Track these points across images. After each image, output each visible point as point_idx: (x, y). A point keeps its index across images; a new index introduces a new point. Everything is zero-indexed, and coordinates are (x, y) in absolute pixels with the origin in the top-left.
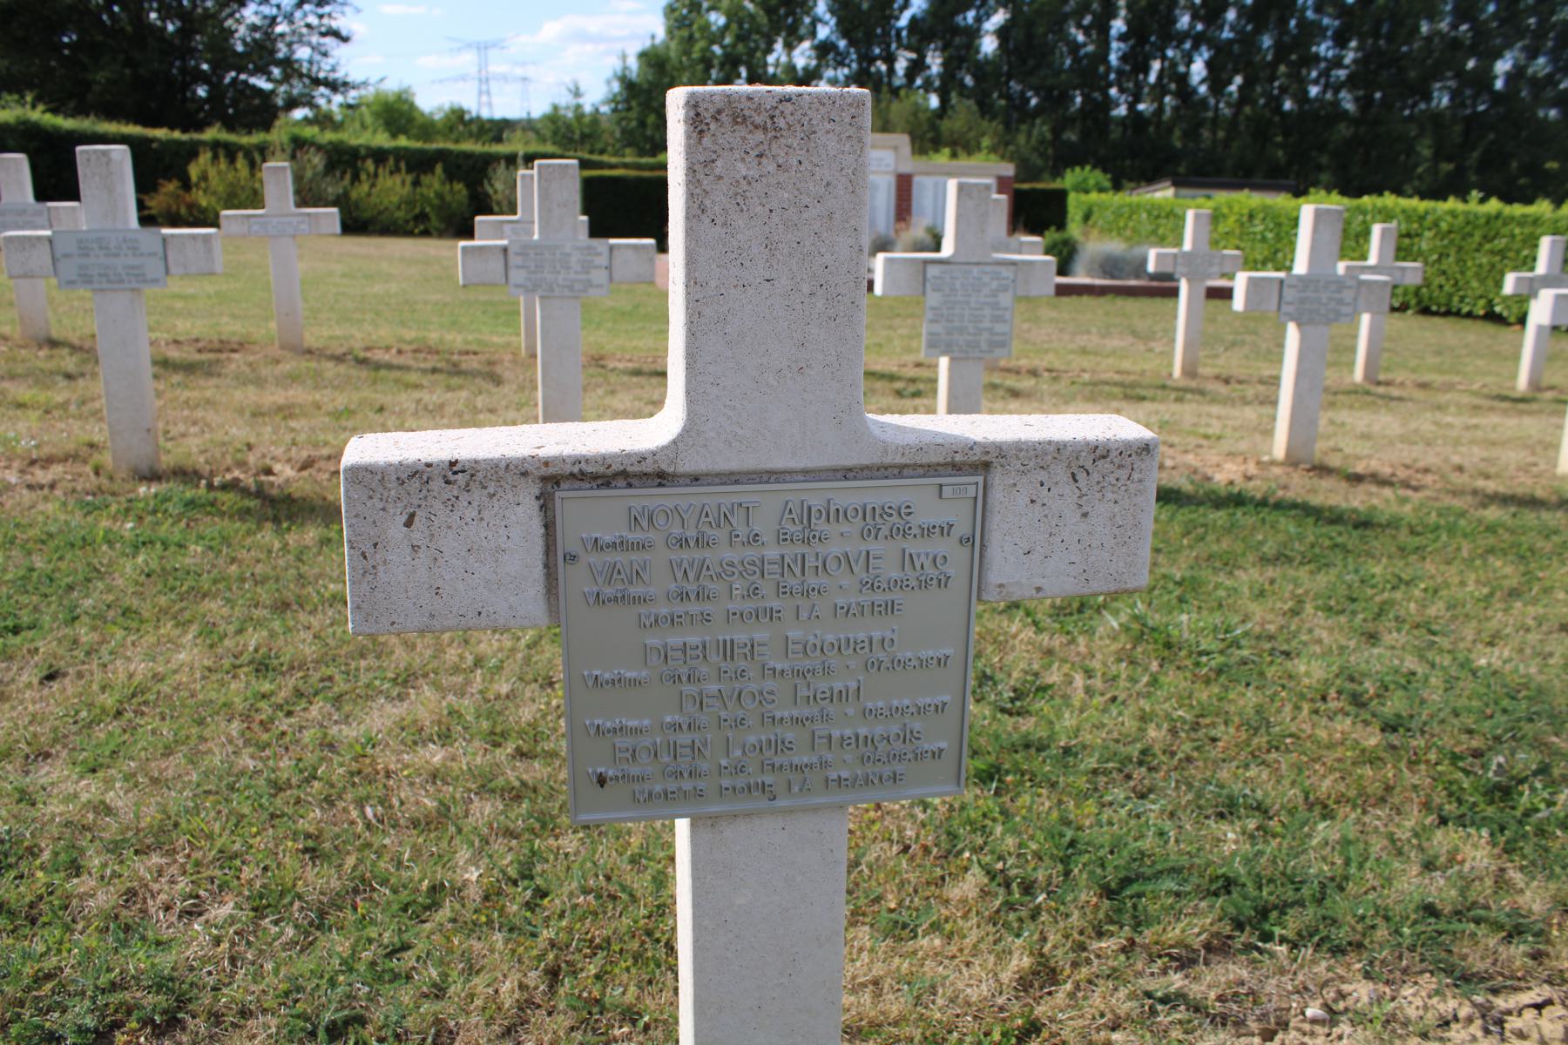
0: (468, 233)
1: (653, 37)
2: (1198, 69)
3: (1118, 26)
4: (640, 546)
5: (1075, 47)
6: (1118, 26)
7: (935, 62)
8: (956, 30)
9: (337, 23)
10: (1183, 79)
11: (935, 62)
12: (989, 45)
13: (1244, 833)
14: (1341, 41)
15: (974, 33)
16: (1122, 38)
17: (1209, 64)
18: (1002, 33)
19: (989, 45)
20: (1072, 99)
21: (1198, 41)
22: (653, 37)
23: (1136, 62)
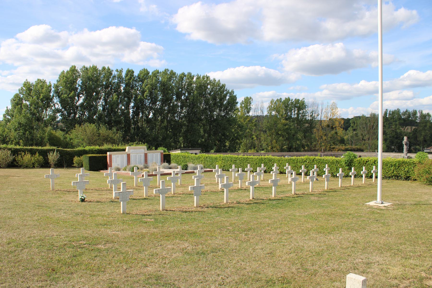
1: (7, 107)
2: (151, 116)
3: (132, 104)
6: (132, 104)
8: (92, 106)
19: (100, 108)
22: (7, 107)
23: (136, 113)
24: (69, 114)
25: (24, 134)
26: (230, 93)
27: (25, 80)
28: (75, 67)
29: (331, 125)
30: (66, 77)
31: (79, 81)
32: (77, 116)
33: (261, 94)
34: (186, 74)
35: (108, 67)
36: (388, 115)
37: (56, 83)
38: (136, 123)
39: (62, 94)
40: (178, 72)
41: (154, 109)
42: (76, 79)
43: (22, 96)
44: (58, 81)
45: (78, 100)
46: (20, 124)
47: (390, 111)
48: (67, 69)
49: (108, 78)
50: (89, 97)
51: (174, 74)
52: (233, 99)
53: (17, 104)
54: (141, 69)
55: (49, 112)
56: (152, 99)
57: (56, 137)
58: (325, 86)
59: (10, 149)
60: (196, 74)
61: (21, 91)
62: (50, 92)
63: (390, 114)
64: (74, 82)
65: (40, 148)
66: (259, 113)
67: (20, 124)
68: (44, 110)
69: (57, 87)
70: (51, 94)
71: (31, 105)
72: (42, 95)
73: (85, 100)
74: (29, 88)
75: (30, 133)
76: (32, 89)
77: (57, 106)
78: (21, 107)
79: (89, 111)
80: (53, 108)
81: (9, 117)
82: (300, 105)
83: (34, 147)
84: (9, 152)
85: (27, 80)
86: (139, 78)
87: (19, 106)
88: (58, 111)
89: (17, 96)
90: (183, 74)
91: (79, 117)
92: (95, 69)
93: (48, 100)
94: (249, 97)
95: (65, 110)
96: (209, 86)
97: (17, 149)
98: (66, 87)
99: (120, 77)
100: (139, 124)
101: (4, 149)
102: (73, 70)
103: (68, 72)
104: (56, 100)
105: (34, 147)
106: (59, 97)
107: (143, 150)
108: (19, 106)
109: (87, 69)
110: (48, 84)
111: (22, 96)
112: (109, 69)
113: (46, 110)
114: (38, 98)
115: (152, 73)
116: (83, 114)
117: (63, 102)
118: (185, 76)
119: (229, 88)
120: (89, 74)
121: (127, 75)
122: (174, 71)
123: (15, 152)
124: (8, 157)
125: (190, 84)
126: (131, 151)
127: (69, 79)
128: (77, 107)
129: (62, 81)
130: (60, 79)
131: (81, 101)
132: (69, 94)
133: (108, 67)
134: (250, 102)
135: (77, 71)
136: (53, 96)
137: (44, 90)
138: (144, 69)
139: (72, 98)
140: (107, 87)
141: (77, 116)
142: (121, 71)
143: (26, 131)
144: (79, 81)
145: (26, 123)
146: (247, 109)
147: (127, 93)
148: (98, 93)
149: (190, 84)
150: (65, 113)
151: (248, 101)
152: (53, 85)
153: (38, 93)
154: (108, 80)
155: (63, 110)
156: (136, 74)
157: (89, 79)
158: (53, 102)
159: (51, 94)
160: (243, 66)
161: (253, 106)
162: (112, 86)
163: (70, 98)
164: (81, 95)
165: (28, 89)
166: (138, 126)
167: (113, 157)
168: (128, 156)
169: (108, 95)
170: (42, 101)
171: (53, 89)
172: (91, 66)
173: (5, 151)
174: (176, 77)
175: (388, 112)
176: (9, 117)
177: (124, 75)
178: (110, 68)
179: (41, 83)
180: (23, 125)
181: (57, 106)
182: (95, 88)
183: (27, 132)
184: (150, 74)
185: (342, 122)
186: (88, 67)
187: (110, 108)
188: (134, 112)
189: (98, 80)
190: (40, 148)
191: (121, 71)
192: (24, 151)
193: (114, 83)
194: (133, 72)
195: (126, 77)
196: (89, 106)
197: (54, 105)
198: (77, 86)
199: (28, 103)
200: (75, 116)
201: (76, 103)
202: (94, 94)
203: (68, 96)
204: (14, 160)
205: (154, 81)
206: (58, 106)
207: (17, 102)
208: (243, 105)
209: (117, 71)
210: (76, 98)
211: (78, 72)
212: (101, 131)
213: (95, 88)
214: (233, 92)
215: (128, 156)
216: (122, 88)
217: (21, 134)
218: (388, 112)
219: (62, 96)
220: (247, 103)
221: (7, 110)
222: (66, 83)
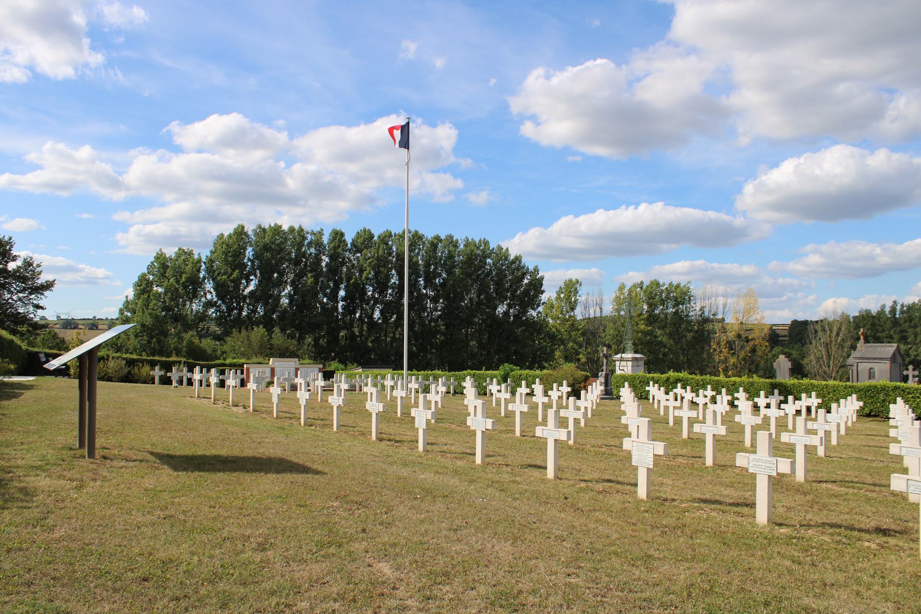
0: (414, 418)
1: (127, 297)
2: (377, 314)
3: (342, 293)
4: (715, 422)
5: (322, 303)
6: (342, 293)
7: (261, 310)
8: (271, 296)
9: (41, 303)
10: (371, 317)
11: (261, 310)
12: (285, 301)
13: (803, 345)
14: (435, 300)
15: (279, 297)
16: (343, 299)
17: (381, 312)
18: (290, 297)
19: (285, 301)
20: (277, 316)
21: (376, 301)
22: (127, 297)
23: (349, 310)
24: (230, 310)
25: (149, 342)
26: (532, 274)
27: (158, 250)
28: (243, 227)
29: (743, 336)
30: (227, 245)
31: (249, 252)
32: (244, 314)
33: (859, 247)
34: (443, 237)
35: (300, 227)
36: (898, 313)
37: (209, 254)
38: (349, 326)
39: (218, 274)
40: (429, 234)
41: (382, 302)
42: (245, 249)
43: (151, 277)
44: (212, 252)
45: (247, 286)
46: (143, 326)
47: (902, 306)
48: (228, 229)
49: (301, 244)
50: (266, 281)
51: (421, 238)
52: (537, 285)
53: (143, 291)
54: (359, 228)
55: (196, 306)
56: (378, 282)
57: (200, 349)
58: (810, 247)
59: (124, 359)
60: (463, 238)
61: (150, 267)
62: (199, 271)
63: (902, 312)
64: (239, 253)
65: (164, 359)
66: (593, 312)
67: (143, 326)
68: (188, 303)
69: (211, 261)
70: (201, 276)
71: (166, 293)
72: (184, 276)
73: (257, 286)
74: (163, 264)
75: (159, 341)
76: (168, 267)
77: (209, 297)
78: (149, 296)
79: (266, 304)
80: (203, 299)
81: (129, 314)
82: (681, 296)
83: (157, 358)
84: (124, 362)
85: (161, 250)
86: (355, 247)
87: (146, 296)
88: (210, 304)
89: (143, 278)
90: (438, 238)
91: (247, 316)
92: (277, 230)
93: (193, 286)
94: (574, 280)
95: (224, 302)
96: (489, 261)
97: (134, 359)
98: (226, 261)
99: (318, 244)
100: (356, 331)
101: (118, 358)
102: (240, 233)
103: (230, 236)
104: (209, 286)
105: (157, 358)
106: (214, 280)
107: (293, 364)
108: (146, 296)
109: (264, 230)
110: (196, 257)
111: (151, 277)
112: (302, 230)
113: (191, 302)
114: (178, 282)
115: (379, 237)
116: (254, 311)
117: (220, 288)
118: (441, 241)
119: (529, 263)
120: (267, 240)
121: (333, 240)
122: (420, 232)
123: (131, 363)
124: (121, 368)
125: (451, 257)
126: (277, 364)
127: (232, 249)
128: (245, 297)
129: (219, 252)
130: (216, 248)
131: (251, 287)
132: (231, 274)
133: (300, 227)
134: (576, 289)
135: (246, 234)
136: (204, 278)
137: (189, 268)
138: (365, 231)
139: (237, 282)
140: (297, 262)
141: (244, 314)
142: (321, 233)
143: (152, 337)
144: (249, 252)
145: (153, 325)
146: (570, 302)
147: (333, 270)
148: (281, 274)
149: (451, 257)
150: (224, 307)
151: (571, 289)
152: (204, 259)
153: (179, 273)
154: (299, 249)
155: (220, 302)
156: (349, 238)
157: (266, 248)
158: (204, 289)
159: (201, 276)
160: (572, 216)
161: (582, 298)
162: (307, 259)
163: (232, 281)
164: (252, 277)
165: (162, 265)
166: (353, 333)
167: (251, 370)
168: (273, 370)
169: (300, 275)
170: (185, 287)
171: (203, 267)
172: (273, 225)
173: (119, 361)
174: (424, 243)
175: (898, 307)
176: (129, 314)
177: (325, 239)
178: (303, 227)
179: (185, 255)
180: (148, 328)
181: (209, 297)
182: (277, 265)
183: (154, 340)
184: (376, 238)
185: (766, 331)
186: (267, 227)
187: (303, 299)
188: (344, 308)
189: (281, 250)
190: (164, 359)
191: (321, 233)
192: (142, 361)
193: (311, 254)
194: (342, 235)
195: (329, 243)
196: (264, 295)
197: (205, 294)
198: (245, 261)
199: (160, 290)
200: (240, 314)
201: (243, 291)
202: (275, 275)
203: (229, 277)
204: (129, 372)
205: (381, 252)
206: (212, 296)
207: (143, 287)
208: (562, 296)
209: (313, 233)
210: (244, 281)
211: (248, 236)
212: (273, 342)
213: (277, 265)
214: (536, 270)
215: (273, 370)
216: (324, 264)
217: (144, 342)
218: (898, 307)
219: (219, 278)
220: (570, 292)
221: (127, 301)
222: (226, 255)
